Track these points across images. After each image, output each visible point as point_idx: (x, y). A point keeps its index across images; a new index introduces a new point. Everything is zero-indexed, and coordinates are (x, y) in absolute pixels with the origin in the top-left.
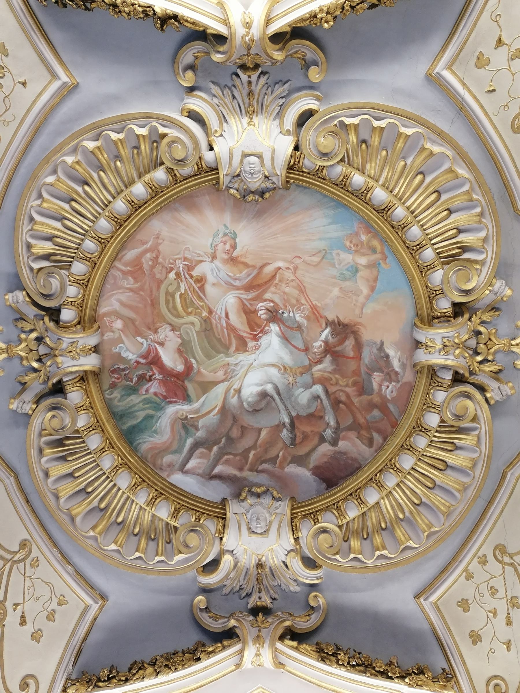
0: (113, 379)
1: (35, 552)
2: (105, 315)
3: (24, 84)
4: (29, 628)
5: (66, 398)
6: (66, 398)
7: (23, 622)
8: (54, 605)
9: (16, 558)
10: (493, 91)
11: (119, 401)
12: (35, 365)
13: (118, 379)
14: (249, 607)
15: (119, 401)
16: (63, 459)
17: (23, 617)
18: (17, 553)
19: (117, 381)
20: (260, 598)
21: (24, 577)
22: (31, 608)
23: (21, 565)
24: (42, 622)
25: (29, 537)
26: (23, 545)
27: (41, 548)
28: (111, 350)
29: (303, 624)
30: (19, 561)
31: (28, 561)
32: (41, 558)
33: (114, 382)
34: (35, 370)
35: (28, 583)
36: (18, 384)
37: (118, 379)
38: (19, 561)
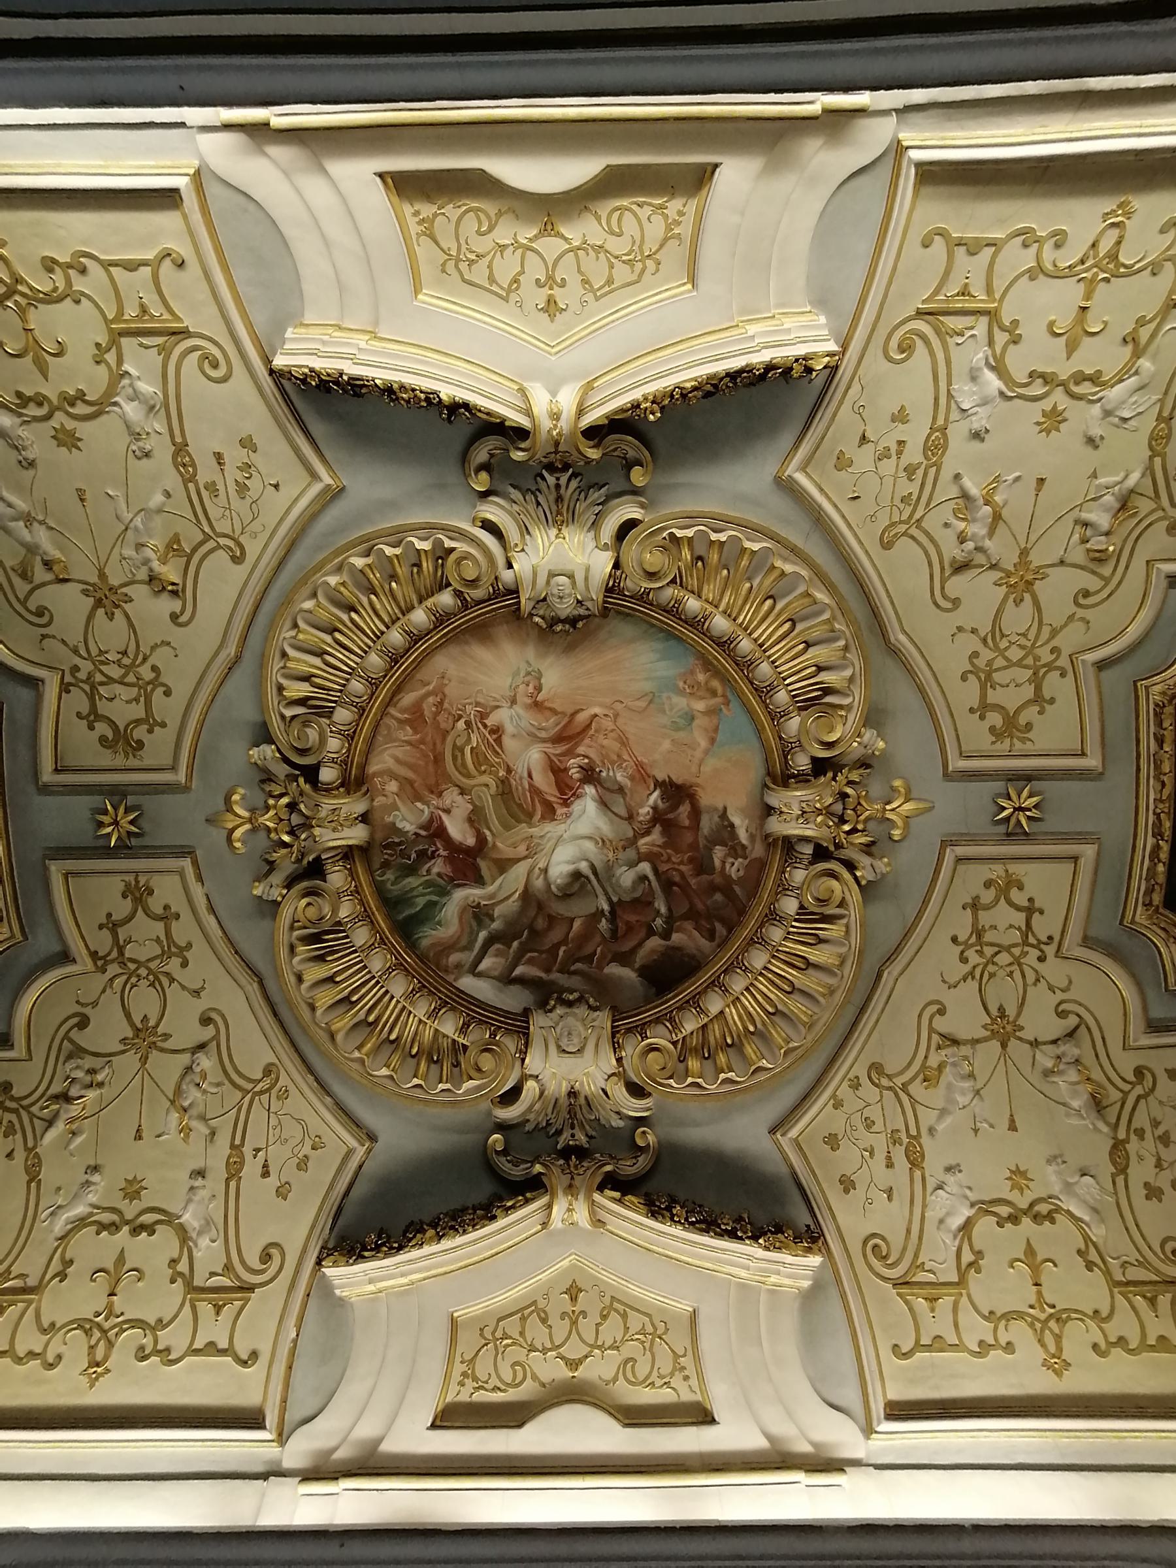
1: (283, 1081)
4: (273, 1181)
7: (266, 1174)
8: (306, 1149)
12: (286, 838)
14: (559, 1147)
17: (265, 1166)
20: (573, 1136)
22: (277, 1154)
24: (290, 1173)
29: (630, 1168)
30: (262, 1092)
31: (274, 1092)
34: (285, 845)
37: (392, 855)
38: (262, 1092)
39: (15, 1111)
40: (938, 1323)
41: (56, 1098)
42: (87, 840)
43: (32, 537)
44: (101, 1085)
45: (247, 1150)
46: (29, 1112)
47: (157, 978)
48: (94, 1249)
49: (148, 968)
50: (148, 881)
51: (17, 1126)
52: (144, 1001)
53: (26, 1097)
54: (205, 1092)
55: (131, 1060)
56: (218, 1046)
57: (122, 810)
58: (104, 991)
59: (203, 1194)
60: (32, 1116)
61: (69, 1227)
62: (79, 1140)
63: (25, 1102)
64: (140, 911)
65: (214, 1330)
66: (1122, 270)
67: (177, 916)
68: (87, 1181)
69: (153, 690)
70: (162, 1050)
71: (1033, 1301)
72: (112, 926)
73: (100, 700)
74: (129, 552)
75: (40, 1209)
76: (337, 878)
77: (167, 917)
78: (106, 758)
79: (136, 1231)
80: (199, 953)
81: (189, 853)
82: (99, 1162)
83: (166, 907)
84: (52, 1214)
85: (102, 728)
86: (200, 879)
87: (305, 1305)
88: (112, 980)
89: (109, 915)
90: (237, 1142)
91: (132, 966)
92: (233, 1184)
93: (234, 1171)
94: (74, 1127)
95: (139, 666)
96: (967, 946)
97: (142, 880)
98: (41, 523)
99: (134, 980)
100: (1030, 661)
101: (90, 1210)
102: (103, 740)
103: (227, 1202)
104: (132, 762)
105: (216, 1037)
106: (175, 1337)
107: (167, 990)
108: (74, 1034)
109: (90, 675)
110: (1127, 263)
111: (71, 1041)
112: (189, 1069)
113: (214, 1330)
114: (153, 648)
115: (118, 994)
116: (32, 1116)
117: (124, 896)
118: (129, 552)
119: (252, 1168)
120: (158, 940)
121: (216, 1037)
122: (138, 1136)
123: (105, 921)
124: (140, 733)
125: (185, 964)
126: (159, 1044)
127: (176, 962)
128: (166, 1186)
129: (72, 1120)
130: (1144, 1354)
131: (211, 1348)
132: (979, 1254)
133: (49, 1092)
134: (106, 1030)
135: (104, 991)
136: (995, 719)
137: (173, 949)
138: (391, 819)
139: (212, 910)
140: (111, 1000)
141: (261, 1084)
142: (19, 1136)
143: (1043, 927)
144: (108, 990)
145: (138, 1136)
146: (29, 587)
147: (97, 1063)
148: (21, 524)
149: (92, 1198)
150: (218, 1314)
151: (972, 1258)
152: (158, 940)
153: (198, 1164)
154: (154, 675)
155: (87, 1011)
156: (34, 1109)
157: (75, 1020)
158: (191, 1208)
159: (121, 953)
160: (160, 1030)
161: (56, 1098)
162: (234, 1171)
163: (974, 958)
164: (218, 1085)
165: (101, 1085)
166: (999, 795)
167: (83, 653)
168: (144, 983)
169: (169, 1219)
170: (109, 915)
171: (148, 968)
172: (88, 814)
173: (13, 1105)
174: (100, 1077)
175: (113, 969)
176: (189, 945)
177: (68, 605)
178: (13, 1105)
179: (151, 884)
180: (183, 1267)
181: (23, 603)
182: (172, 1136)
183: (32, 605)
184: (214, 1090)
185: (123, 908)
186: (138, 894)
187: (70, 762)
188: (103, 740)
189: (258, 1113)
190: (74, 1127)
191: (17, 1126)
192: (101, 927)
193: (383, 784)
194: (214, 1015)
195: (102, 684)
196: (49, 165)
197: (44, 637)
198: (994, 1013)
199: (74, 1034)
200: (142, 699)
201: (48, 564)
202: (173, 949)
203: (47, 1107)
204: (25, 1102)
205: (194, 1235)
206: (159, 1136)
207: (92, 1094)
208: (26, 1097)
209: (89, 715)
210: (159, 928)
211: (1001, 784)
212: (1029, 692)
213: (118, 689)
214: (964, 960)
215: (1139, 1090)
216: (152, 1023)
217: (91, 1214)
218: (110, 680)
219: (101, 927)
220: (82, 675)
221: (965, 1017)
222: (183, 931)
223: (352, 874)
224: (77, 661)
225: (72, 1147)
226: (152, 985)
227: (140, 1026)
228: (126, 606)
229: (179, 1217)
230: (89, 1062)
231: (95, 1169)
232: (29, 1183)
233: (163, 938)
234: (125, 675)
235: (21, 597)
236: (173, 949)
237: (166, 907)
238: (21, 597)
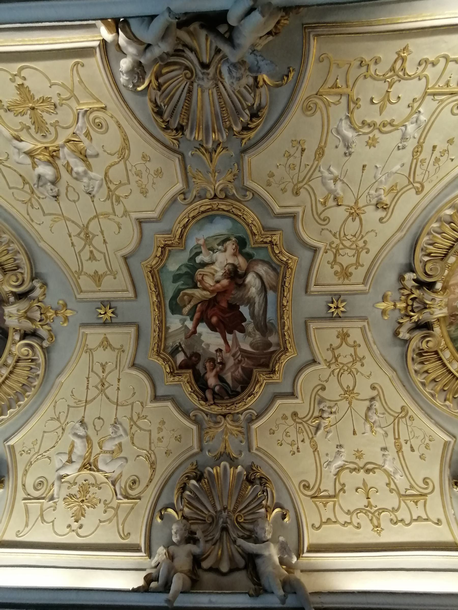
0: (452, 320)
1: (410, 413)
2: (453, 285)
3: (452, 160)
4: (417, 454)
5: (433, 331)
6: (433, 331)
7: (413, 450)
8: (427, 441)
9: (400, 416)
10: (364, 166)
11: (454, 332)
13: (454, 320)
15: (454, 332)
16: (422, 363)
17: (411, 447)
18: (401, 413)
19: (453, 321)
21: (407, 426)
22: (415, 443)
23: (404, 420)
24: (423, 450)
25: (405, 405)
26: (403, 408)
27: (413, 409)
28: (452, 304)
30: (402, 417)
31: (407, 417)
32: (414, 416)
33: (452, 322)
35: (410, 430)
36: (397, 324)
37: (454, 320)
38: (402, 417)
39: (301, 423)
40: (327, 513)
41: (317, 418)
42: (323, 314)
43: (335, 187)
44: (335, 413)
45: (402, 441)
46: (307, 424)
47: (351, 371)
48: (352, 479)
49: (347, 367)
50: (347, 331)
51: (303, 429)
52: (347, 380)
53: (304, 418)
54: (378, 417)
55: (344, 404)
56: (380, 398)
57: (339, 301)
58: (330, 375)
59: (389, 458)
60: (309, 425)
61: (338, 470)
62: (330, 435)
63: (305, 420)
64: (344, 344)
65: (418, 511)
66: (406, 76)
67: (360, 346)
68: (338, 451)
69: (362, 251)
70: (357, 399)
71: (366, 504)
72: (332, 349)
73: (339, 256)
74: (372, 192)
75: (322, 464)
76: (437, 330)
77: (355, 345)
78: (335, 280)
79: (368, 471)
80: (368, 360)
81: (366, 319)
82: (341, 443)
83: (355, 342)
84: (328, 465)
85: (337, 268)
86: (370, 330)
87: (451, 501)
88: (333, 371)
89: (331, 345)
90: (397, 437)
91: (341, 366)
92: (400, 454)
93: (399, 449)
94: (327, 429)
95: (359, 241)
96: (363, 248)
97: (345, 330)
98: (341, 180)
99: (342, 371)
100: (354, 246)
101: (344, 463)
102: (336, 273)
103: (400, 461)
104: (346, 281)
105: (378, 394)
106: (403, 514)
107: (356, 376)
108: (320, 392)
109: (337, 245)
110: (410, 74)
111: (319, 395)
112: (369, 409)
113: (418, 511)
114: (367, 233)
115: (336, 376)
116: (309, 425)
117: (338, 337)
118: (372, 192)
119: (406, 448)
120: (351, 355)
121: (378, 394)
122: (354, 433)
123: (329, 347)
124: (351, 270)
125: (362, 365)
126: (356, 397)
127: (359, 364)
128: (372, 454)
129: (326, 427)
130: (349, 526)
131: (419, 519)
132: (344, 485)
133: (314, 416)
134: (333, 391)
135: (330, 375)
136: (350, 340)
137: (357, 359)
138: (455, 304)
139: (375, 343)
140: (333, 379)
141: (401, 414)
142: (305, 433)
143: (330, 256)
144: (332, 375)
145: (354, 433)
146: (324, 208)
147: (332, 404)
148: (332, 181)
149: (343, 458)
150: (416, 505)
151: (341, 487)
152: (351, 355)
153: (383, 445)
154: (364, 244)
155: (324, 383)
156: (309, 422)
157: (319, 387)
158: (387, 463)
159: (337, 360)
160: (355, 391)
161: (317, 418)
162: (399, 449)
163: (361, 244)
164: (383, 414)
165: (335, 413)
166: (328, 302)
167: (338, 236)
168: (346, 373)
169: (380, 467)
170: (331, 345)
171: (347, 367)
172: (325, 303)
173: (300, 421)
174: (333, 410)
175: (333, 367)
176: (364, 357)
177: (338, 215)
178: (300, 421)
179: (349, 332)
180: (393, 486)
181: (319, 216)
182: (368, 433)
183: (322, 216)
184: (382, 416)
185: (337, 342)
186: (344, 336)
187: (320, 282)
188: (336, 273)
189: (402, 426)
190: (327, 429)
191: (303, 429)
192: (328, 350)
193: (455, 289)
194: (376, 386)
195: (342, 249)
196: (59, 39)
197: (323, 229)
198: (357, 219)
199: (320, 392)
200: (356, 255)
201: (335, 199)
202: (357, 359)
203: (314, 422)
204: (305, 420)
205: (392, 474)
206: (363, 433)
207: (332, 416)
208: (304, 418)
209: (332, 262)
210: (352, 350)
211: (330, 297)
212: (354, 260)
213: (348, 251)
214: (365, 242)
215: (300, 185)
216: (351, 388)
217: (345, 465)
218: (345, 247)
219: (328, 350)
220: (334, 246)
221: (371, 215)
222: (362, 351)
223: (441, 328)
224: (334, 239)
225: (328, 437)
226: (349, 373)
227: (346, 390)
228: (362, 216)
229: (383, 466)
230: (328, 404)
231: (341, 446)
232: (314, 452)
233: (353, 354)
234: (352, 245)
235: (319, 212)
236: (356, 359)
237: (355, 342)
238: (319, 212)
